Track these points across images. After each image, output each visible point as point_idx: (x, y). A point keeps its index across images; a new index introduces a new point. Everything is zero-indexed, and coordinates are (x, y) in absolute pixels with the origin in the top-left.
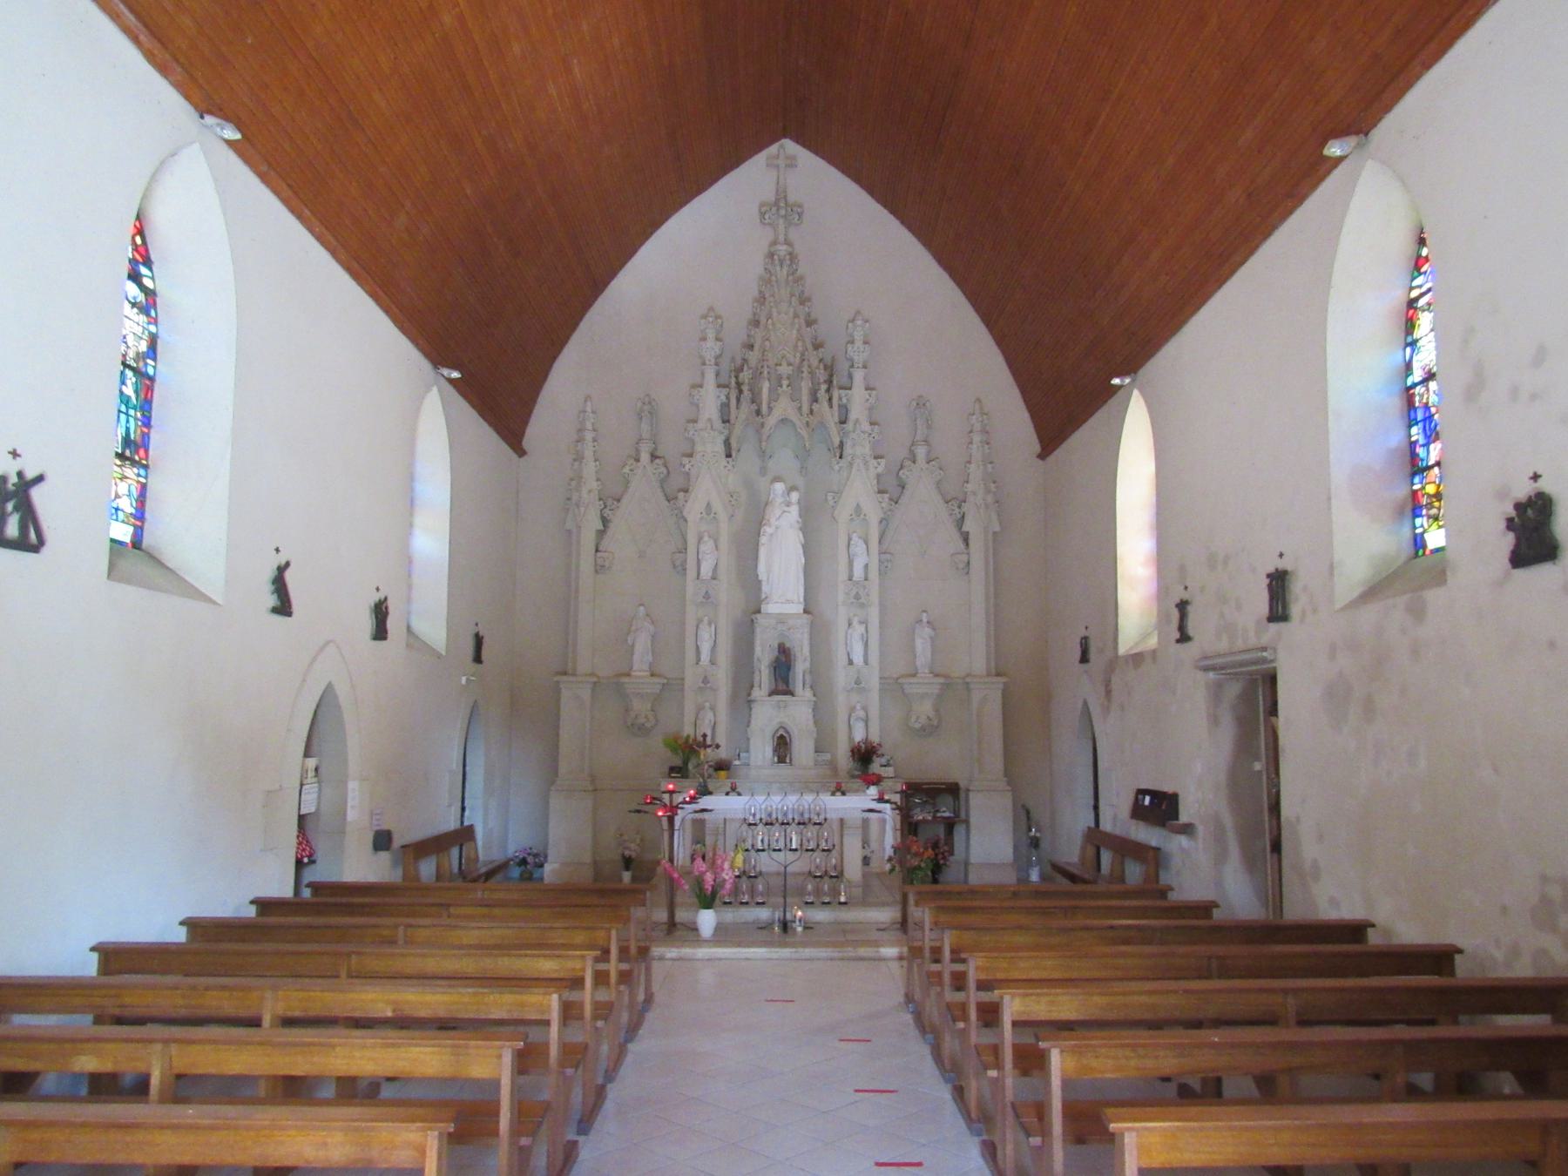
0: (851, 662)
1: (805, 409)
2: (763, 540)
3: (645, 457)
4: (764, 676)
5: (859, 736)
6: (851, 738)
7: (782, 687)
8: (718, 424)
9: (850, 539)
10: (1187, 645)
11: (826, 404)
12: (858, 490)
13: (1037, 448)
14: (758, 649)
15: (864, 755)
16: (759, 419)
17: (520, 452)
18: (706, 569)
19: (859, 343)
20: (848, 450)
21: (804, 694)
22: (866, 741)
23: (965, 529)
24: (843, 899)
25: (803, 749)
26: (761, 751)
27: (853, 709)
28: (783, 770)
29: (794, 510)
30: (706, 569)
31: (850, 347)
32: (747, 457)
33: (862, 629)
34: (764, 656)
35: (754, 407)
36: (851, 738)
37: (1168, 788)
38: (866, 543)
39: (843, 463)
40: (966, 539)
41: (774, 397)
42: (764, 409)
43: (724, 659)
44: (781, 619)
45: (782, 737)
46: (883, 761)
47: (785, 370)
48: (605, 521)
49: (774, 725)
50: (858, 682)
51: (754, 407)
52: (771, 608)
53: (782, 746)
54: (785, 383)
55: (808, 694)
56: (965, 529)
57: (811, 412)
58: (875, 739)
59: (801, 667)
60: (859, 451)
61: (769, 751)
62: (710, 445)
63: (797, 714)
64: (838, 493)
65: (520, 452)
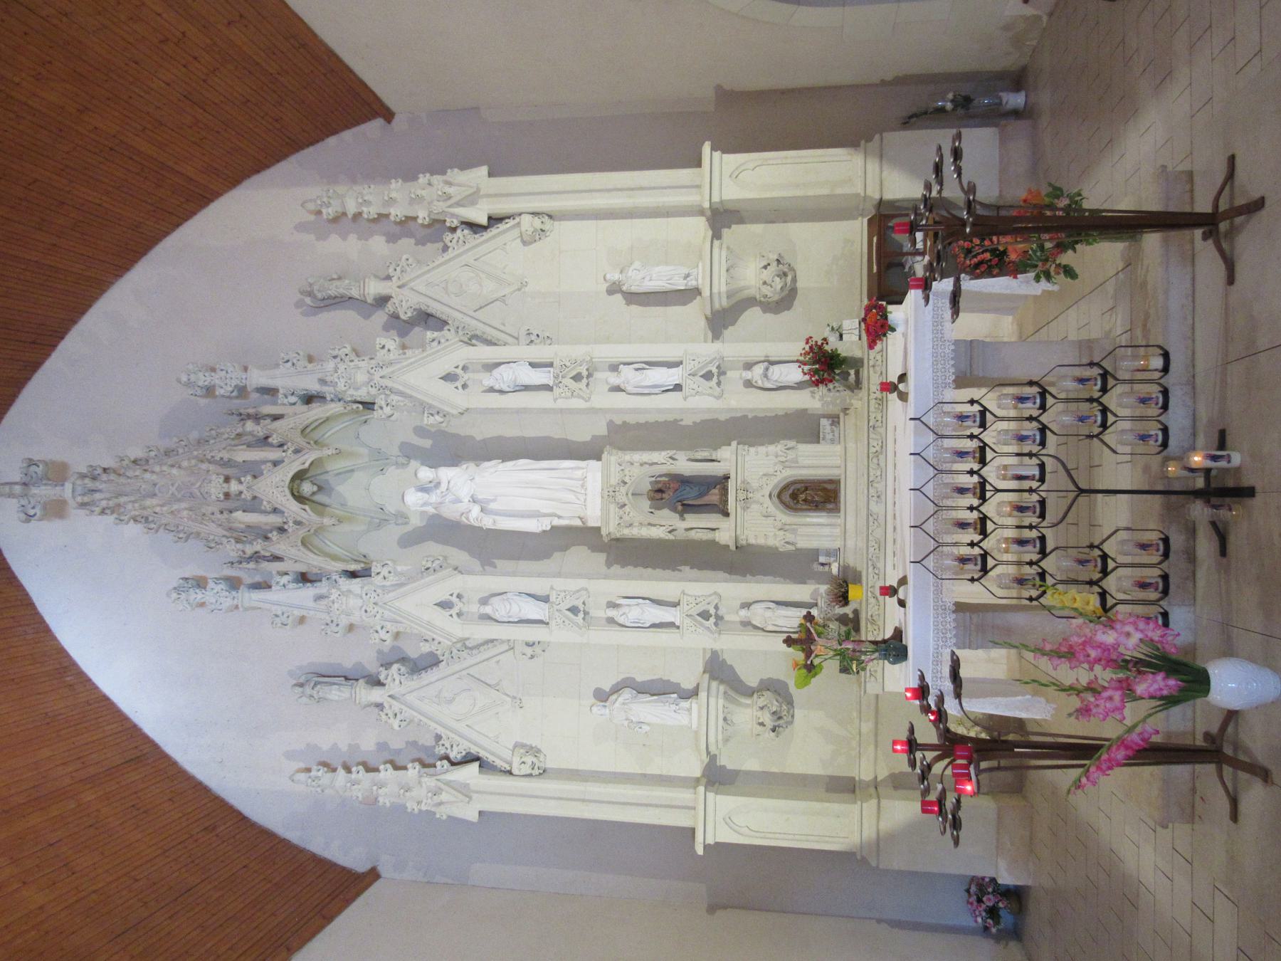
0: (678, 388)
1: (275, 454)
2: (487, 522)
3: (377, 695)
4: (696, 526)
5: (795, 374)
6: (799, 386)
7: (714, 496)
8: (322, 588)
9: (491, 390)
10: (910, 640)
11: (277, 424)
12: (422, 373)
13: (378, 123)
14: (658, 533)
15: (826, 365)
16: (290, 527)
17: (373, 875)
18: (533, 610)
19: (216, 379)
20: (362, 394)
21: (727, 459)
22: (722, 202)
23: (484, 221)
24: (1158, 363)
25: (813, 461)
26: (814, 531)
27: (749, 384)
28: (850, 495)
29: (446, 473)
30: (533, 610)
31: (219, 392)
32: (378, 546)
33: (627, 372)
34: (665, 525)
35: (274, 536)
36: (799, 386)
37: (844, 675)
38: (498, 365)
39: (380, 401)
40: (494, 220)
41: (253, 505)
42: (275, 520)
43: (667, 586)
44: (610, 494)
45: (794, 496)
46: (833, 339)
47: (216, 487)
48: (470, 759)
49: (772, 507)
50: (708, 376)
51: (274, 536)
52: (593, 512)
53: (814, 495)
54: (234, 487)
55: (726, 453)
56: (484, 221)
57: (281, 445)
58: (797, 348)
59: (684, 465)
60: (361, 377)
61: (817, 519)
62: (351, 599)
63: (757, 469)
64: (424, 407)
65: (373, 875)
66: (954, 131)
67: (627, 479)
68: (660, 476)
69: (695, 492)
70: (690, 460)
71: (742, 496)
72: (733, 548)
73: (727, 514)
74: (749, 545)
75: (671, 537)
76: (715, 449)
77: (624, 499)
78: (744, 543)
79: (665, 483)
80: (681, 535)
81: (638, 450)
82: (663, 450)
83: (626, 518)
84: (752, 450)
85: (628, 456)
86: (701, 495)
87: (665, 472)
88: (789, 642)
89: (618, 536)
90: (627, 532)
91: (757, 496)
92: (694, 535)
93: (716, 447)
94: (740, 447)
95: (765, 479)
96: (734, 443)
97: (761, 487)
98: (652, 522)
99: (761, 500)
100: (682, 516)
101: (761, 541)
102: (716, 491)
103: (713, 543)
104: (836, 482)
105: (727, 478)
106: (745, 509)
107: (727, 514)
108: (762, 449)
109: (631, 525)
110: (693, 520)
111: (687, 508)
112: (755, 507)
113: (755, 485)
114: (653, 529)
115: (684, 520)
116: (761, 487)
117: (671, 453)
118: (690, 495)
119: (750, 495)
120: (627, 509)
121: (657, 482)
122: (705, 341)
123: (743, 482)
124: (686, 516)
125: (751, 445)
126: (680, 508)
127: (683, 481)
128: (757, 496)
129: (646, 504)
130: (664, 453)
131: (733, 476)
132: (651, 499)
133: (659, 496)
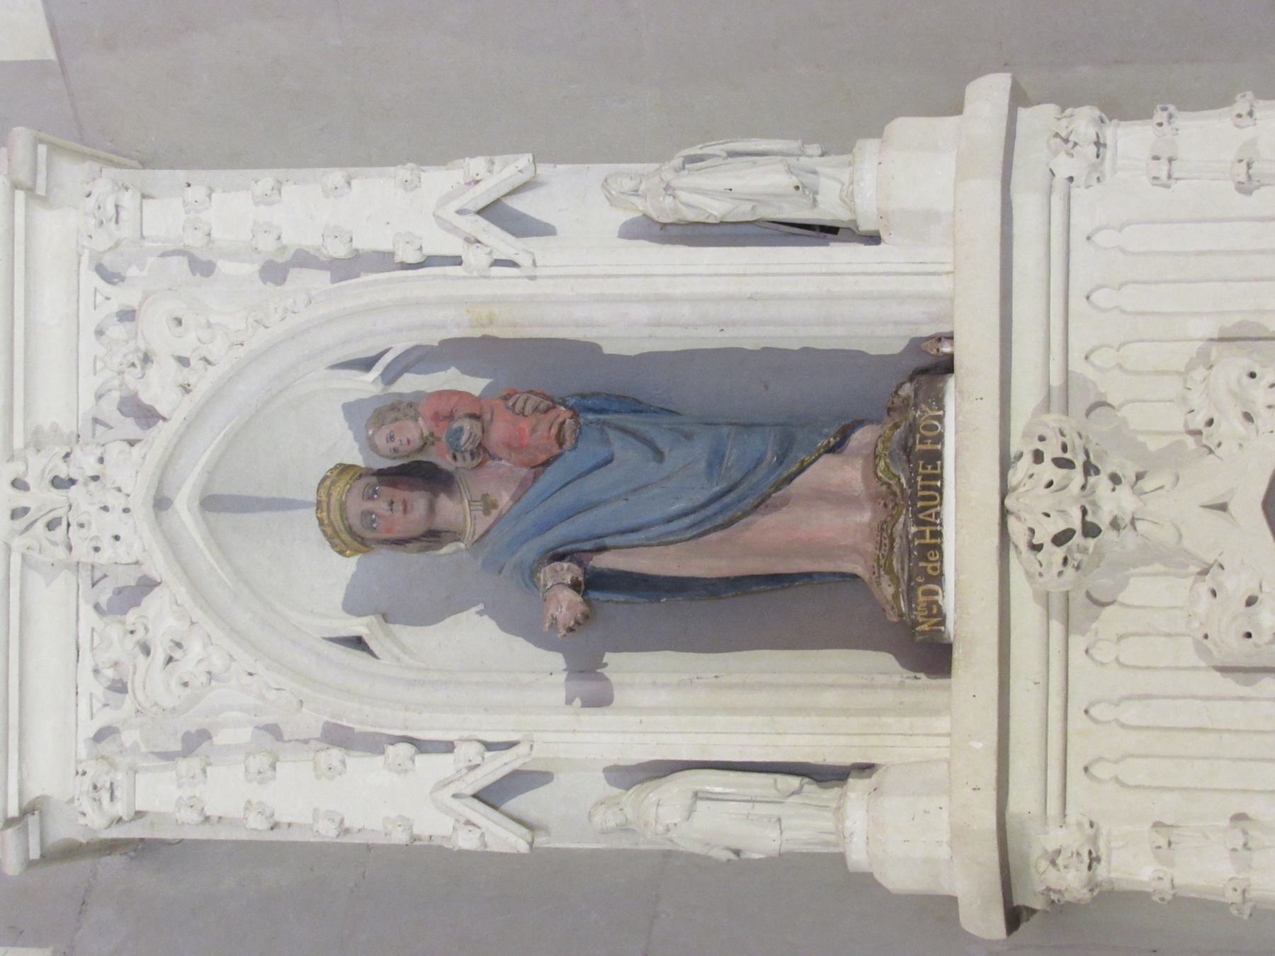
7: (827, 514)
14: (403, 802)
66: (535, 754)
67: (157, 389)
68: (421, 358)
69: (684, 477)
70: (632, 232)
71: (1044, 505)
72: (984, 920)
73: (933, 656)
74: (1112, 900)
75: (504, 837)
76: (839, 141)
77: (135, 544)
78: (1071, 881)
79: (446, 409)
80: (577, 814)
81: (235, 159)
82: (442, 158)
83: (155, 686)
84: (1132, 140)
85: (174, 209)
86: (726, 509)
87: (455, 324)
88: (878, 209)
89: (94, 821)
90: (164, 799)
91: (1171, 509)
92: (686, 820)
93: (844, 130)
94: (1038, 120)
95: (1233, 365)
96: (988, 94)
97: (1201, 433)
98: (359, 718)
99: (1205, 536)
100: (586, 672)
101: (1206, 869)
102: (843, 473)
103: (827, 881)
104: (878, 232)
105: (932, 366)
106: (1069, 613)
107: (933, 656)
108: (1206, 137)
109: (195, 741)
110: (675, 702)
111: (613, 601)
112: (1147, 591)
113: (1152, 417)
114: (366, 772)
115: (600, 700)
116: (1201, 433)
117: (497, 174)
118: (642, 501)
119: (1111, 502)
120: (160, 615)
121: (389, 411)
122: (949, 687)
123: (1060, 396)
124: (619, 665)
125: (1117, 108)
126: (566, 604)
127: (589, 404)
128: (1171, 509)
129: (322, 577)
130: (439, 181)
131: (974, 354)
132: (350, 537)
133: (415, 508)
